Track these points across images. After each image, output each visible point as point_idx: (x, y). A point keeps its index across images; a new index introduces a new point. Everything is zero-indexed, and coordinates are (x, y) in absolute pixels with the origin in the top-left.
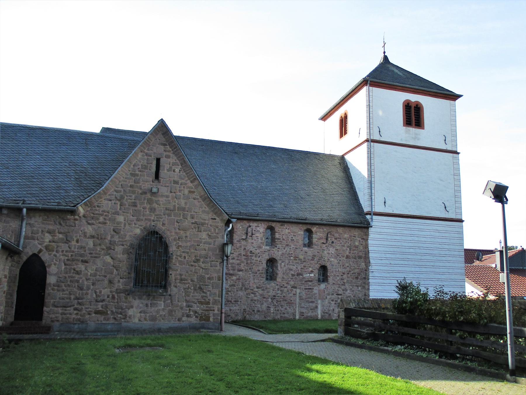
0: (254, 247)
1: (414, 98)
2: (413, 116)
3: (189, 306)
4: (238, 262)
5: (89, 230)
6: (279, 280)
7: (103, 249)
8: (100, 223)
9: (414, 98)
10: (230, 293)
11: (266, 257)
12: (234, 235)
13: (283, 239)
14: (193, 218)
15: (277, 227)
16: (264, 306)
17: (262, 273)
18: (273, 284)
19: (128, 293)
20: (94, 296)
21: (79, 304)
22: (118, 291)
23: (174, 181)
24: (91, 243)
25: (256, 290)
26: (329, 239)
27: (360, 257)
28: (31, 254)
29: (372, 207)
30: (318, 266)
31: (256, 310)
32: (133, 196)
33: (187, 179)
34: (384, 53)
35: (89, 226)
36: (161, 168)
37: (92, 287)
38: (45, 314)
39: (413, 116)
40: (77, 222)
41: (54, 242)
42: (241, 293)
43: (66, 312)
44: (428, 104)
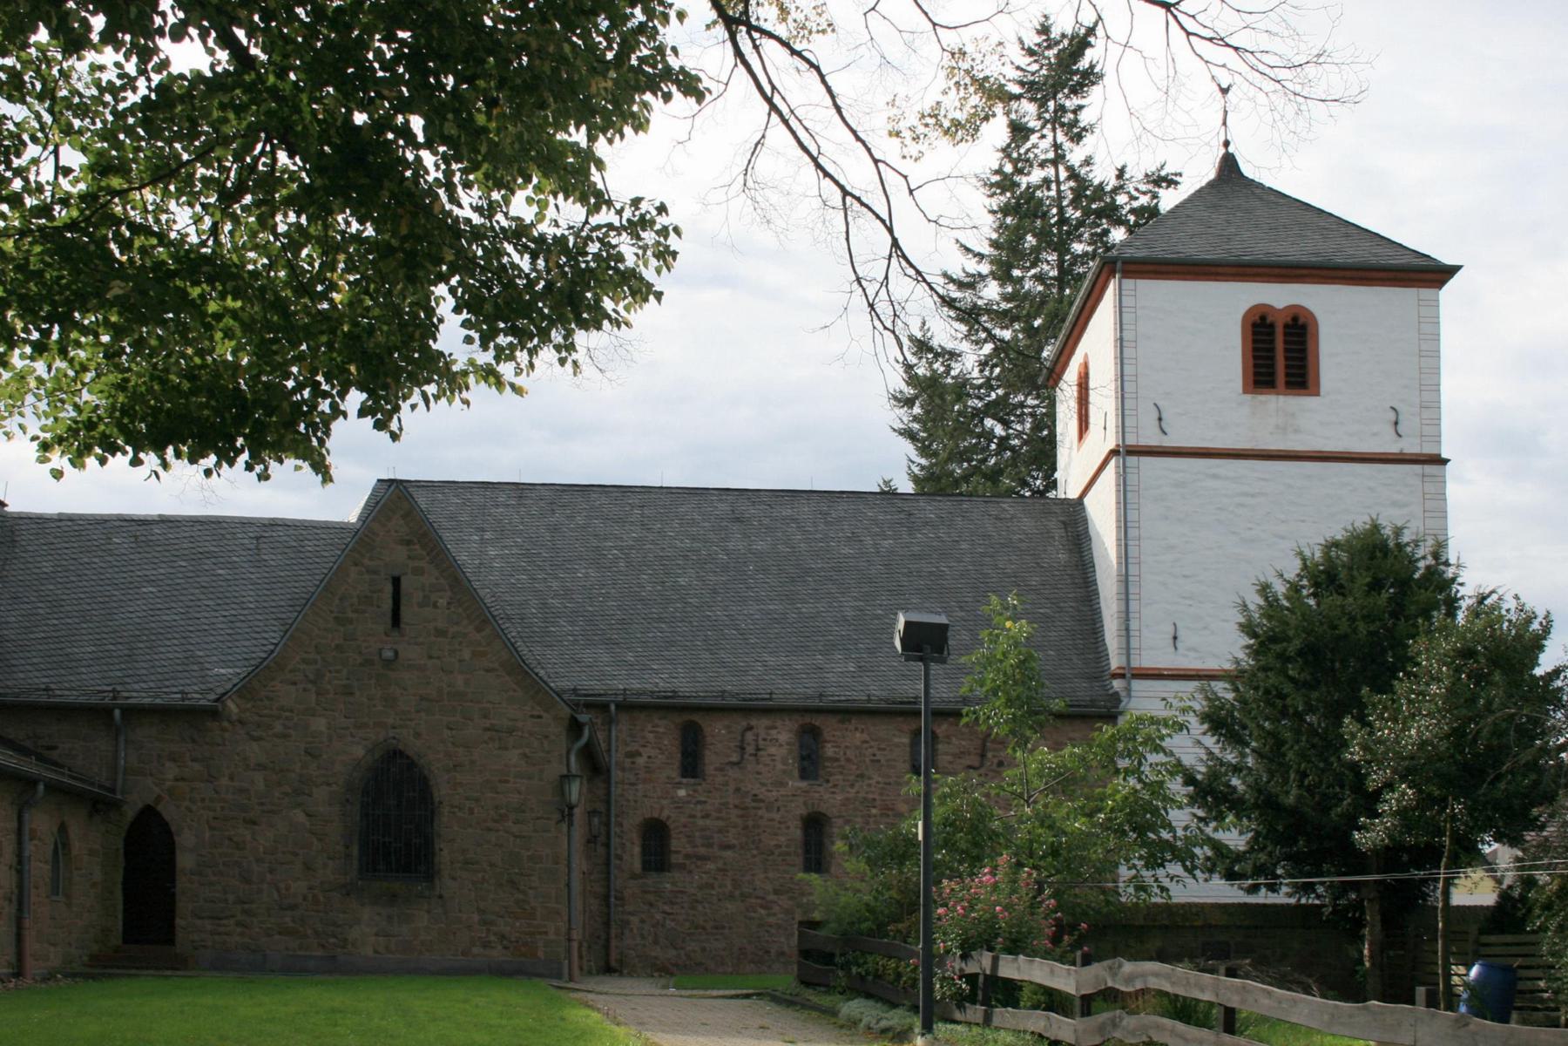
0: (763, 785)
1: (1279, 296)
2: (1280, 356)
3: (484, 922)
4: (721, 823)
7: (287, 794)
8: (276, 736)
9: (1279, 296)
10: (700, 908)
11: (799, 809)
12: (707, 753)
13: (848, 760)
14: (485, 717)
15: (829, 727)
17: (788, 854)
20: (276, 896)
21: (245, 912)
23: (436, 629)
25: (772, 897)
26: (990, 755)
28: (140, 805)
29: (1128, 655)
31: (773, 951)
32: (345, 672)
33: (465, 622)
34: (1227, 144)
35: (255, 745)
36: (403, 601)
37: (269, 876)
38: (180, 935)
39: (1280, 356)
40: (227, 735)
41: (183, 779)
42: (731, 907)
43: (222, 929)
44: (1341, 316)
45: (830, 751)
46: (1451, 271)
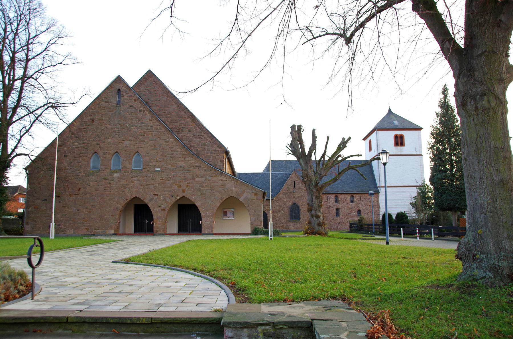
1: (399, 133)
2: (399, 141)
5: (277, 204)
6: (341, 216)
9: (399, 133)
11: (335, 207)
15: (339, 196)
16: (336, 227)
18: (339, 218)
19: (289, 221)
22: (287, 221)
24: (278, 208)
27: (375, 205)
30: (357, 210)
39: (399, 141)
44: (407, 135)
45: (339, 199)
46: (422, 128)
